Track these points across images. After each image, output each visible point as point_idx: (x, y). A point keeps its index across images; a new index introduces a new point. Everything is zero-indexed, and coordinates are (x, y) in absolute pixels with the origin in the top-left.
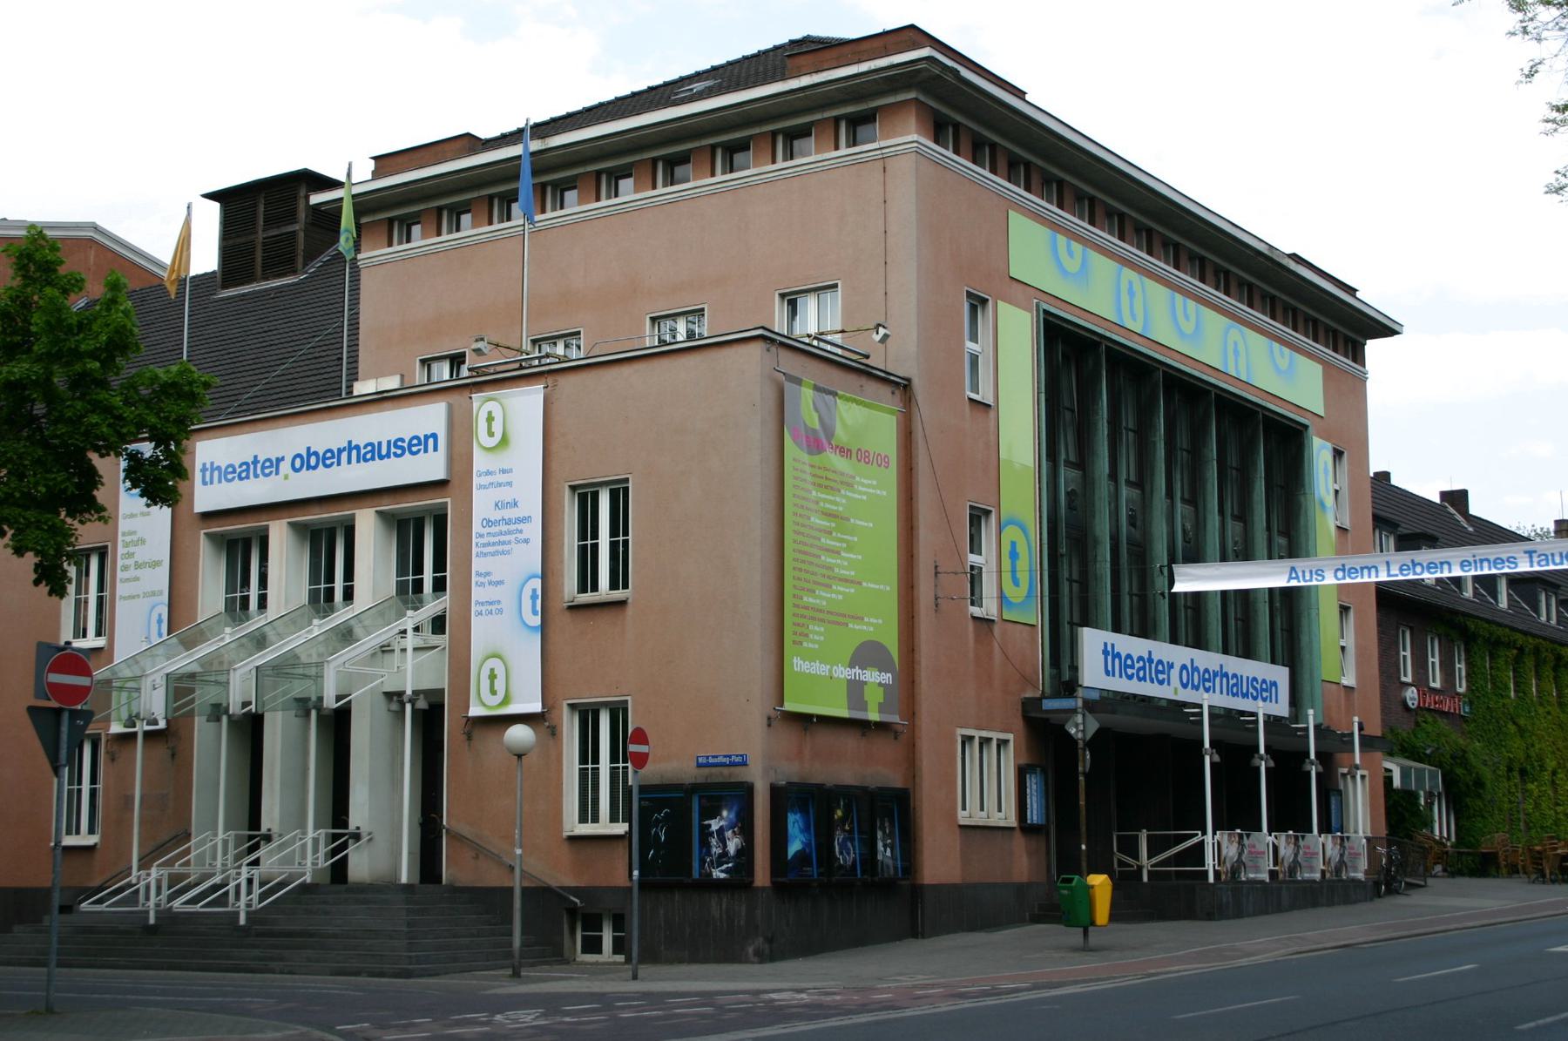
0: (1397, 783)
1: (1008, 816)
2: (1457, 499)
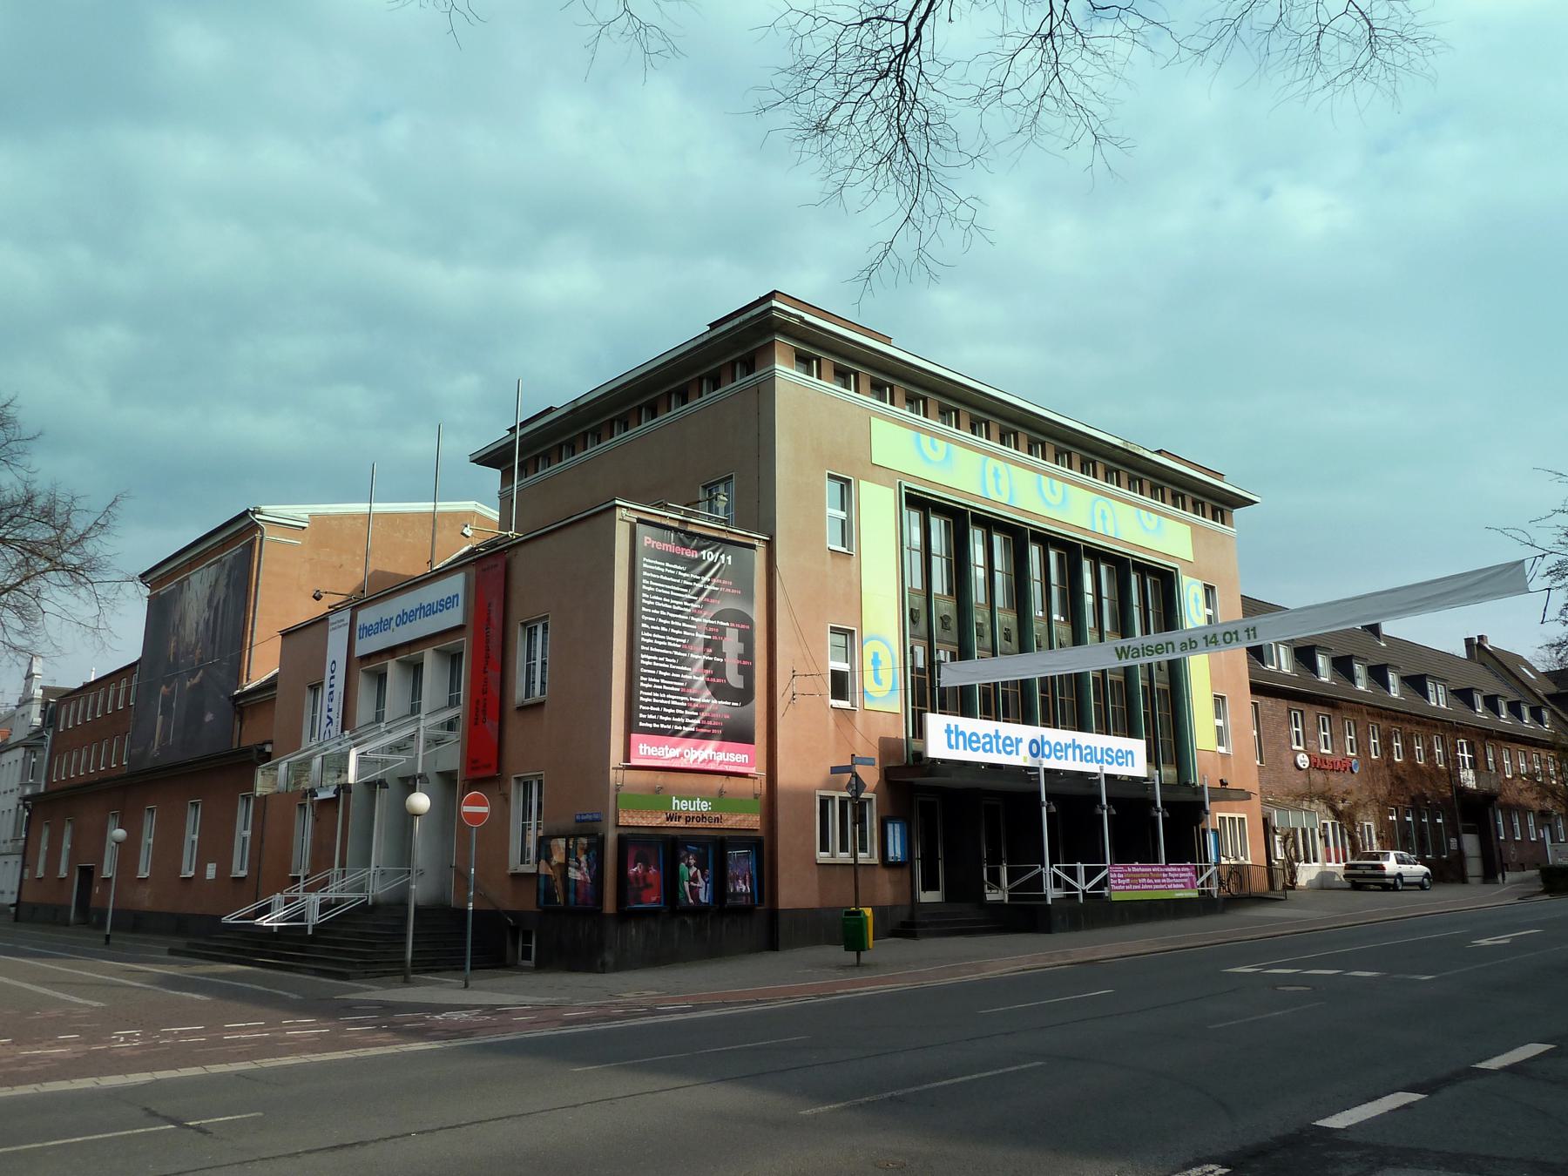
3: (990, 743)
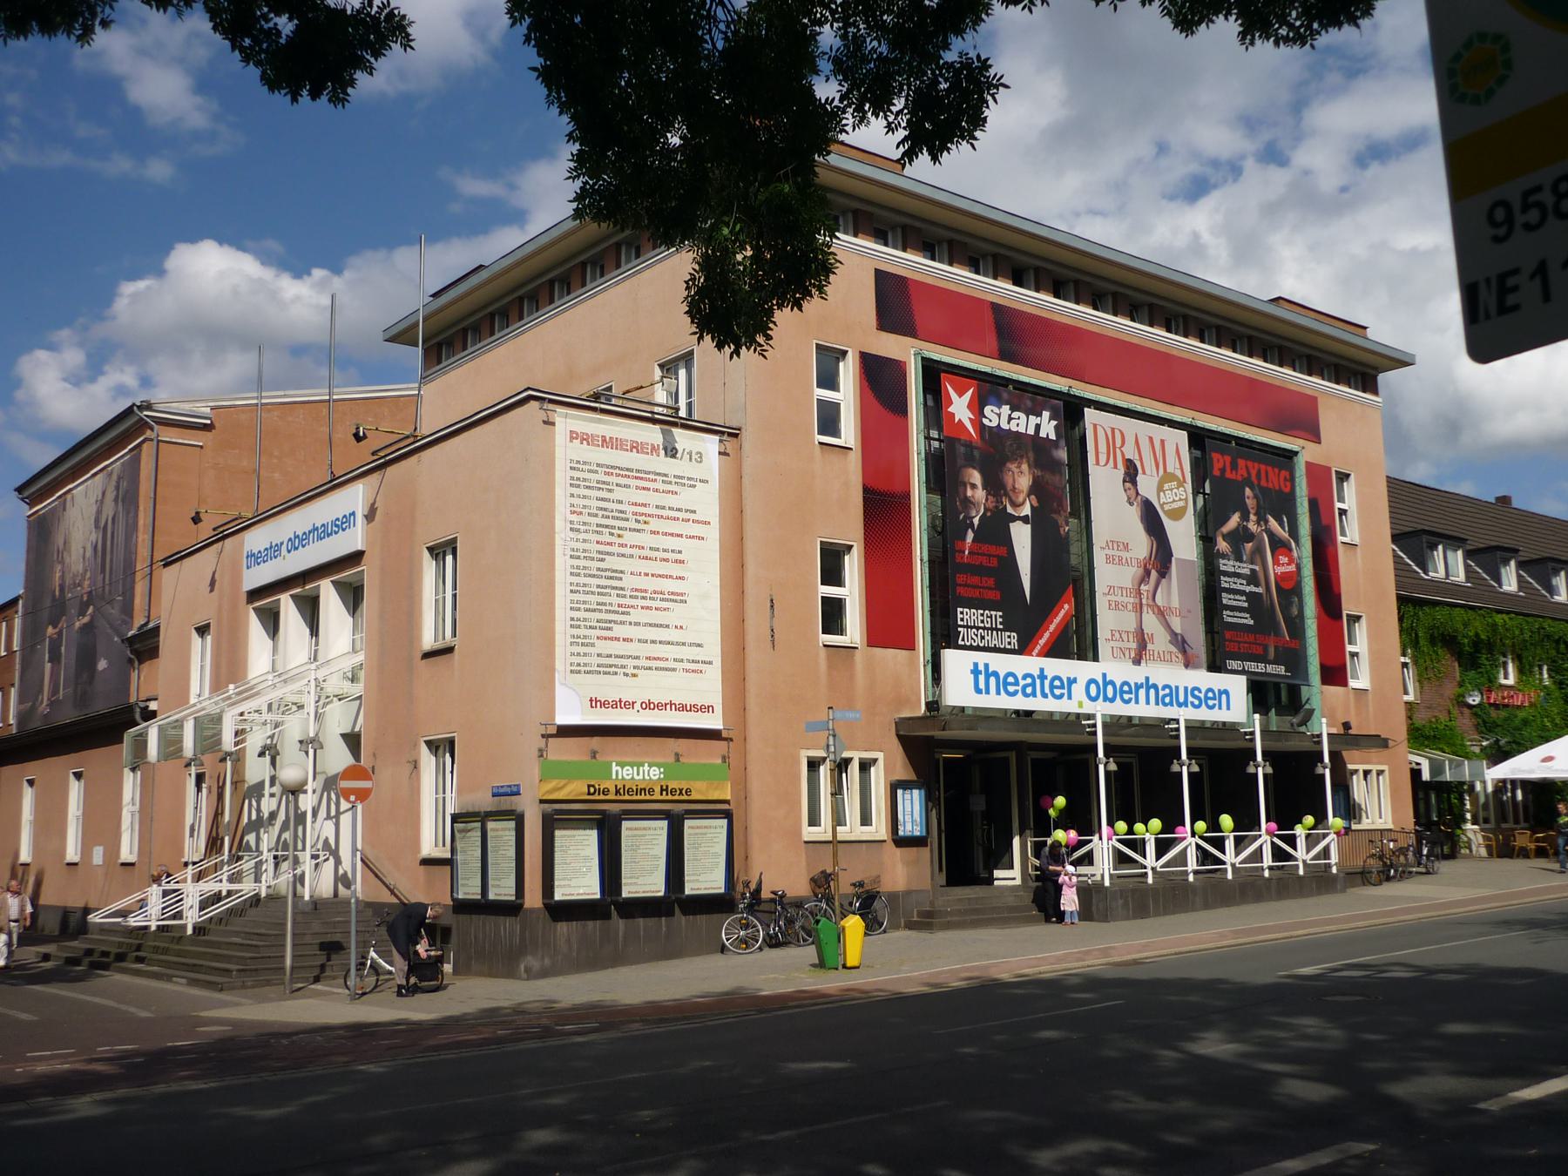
0: (1426, 776)
1: (879, 829)
2: (1504, 500)
3: (1033, 684)
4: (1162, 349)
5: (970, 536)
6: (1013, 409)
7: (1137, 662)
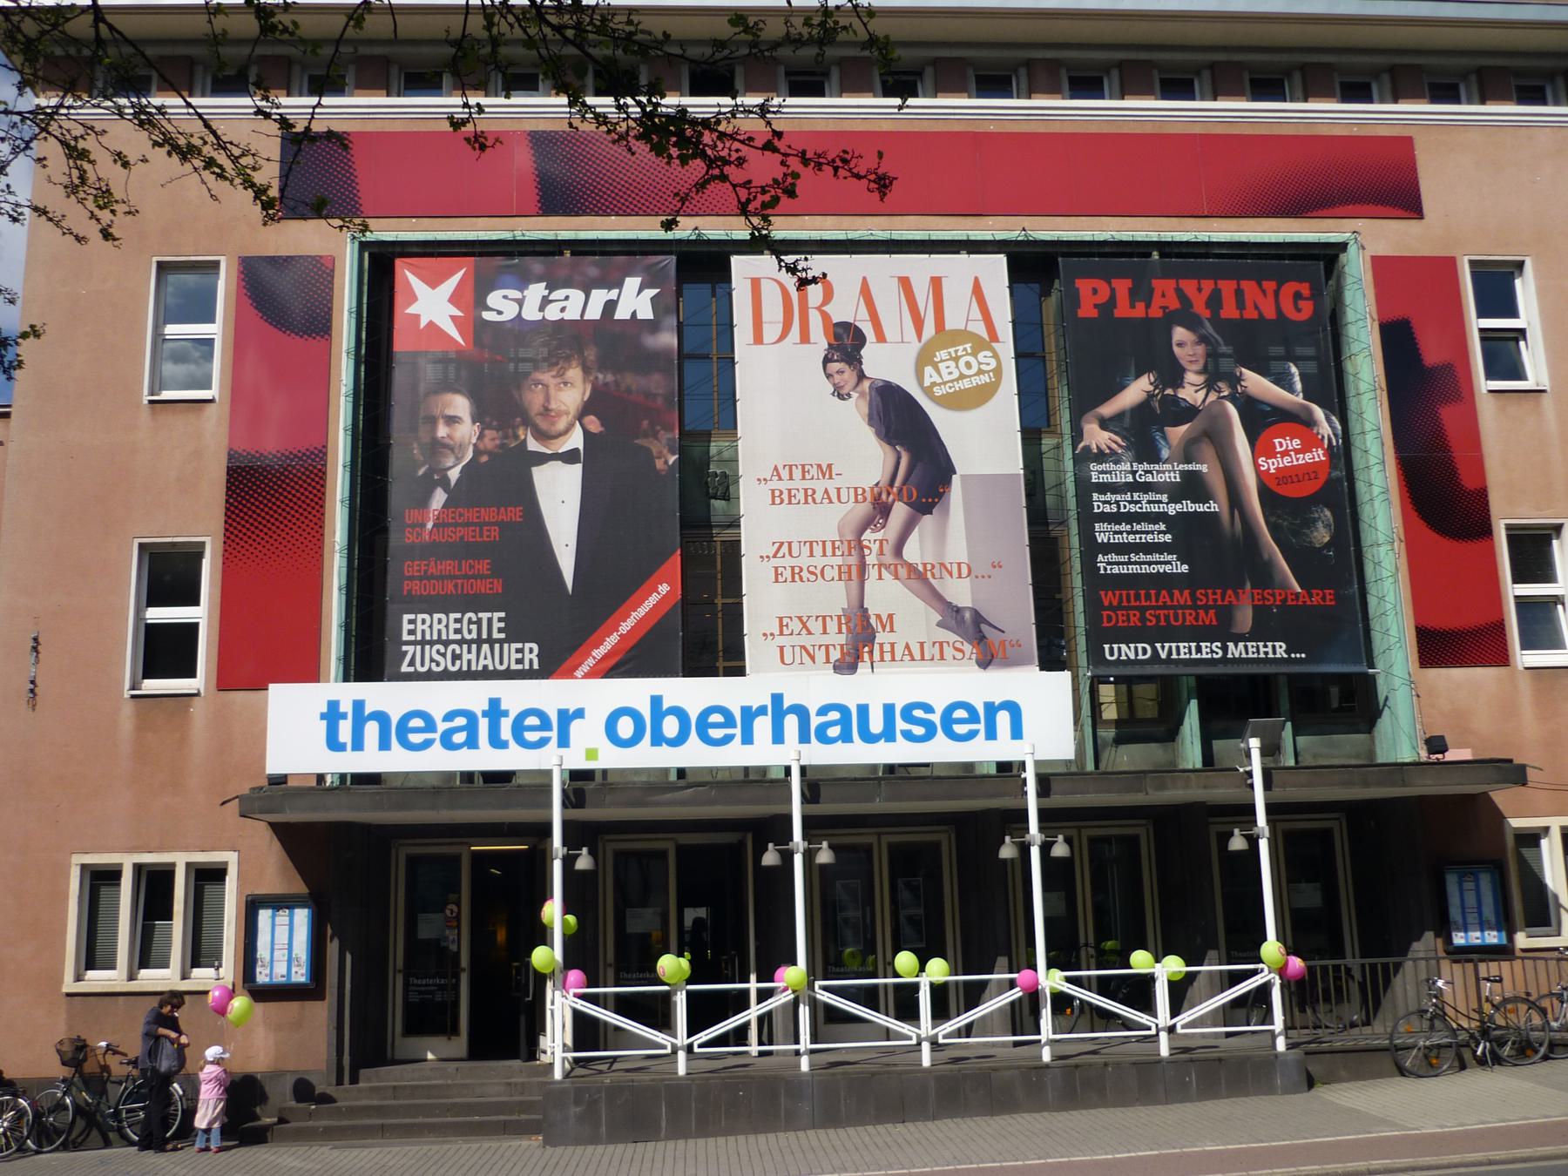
4: (1148, 129)
5: (439, 498)
6: (551, 288)
7: (847, 665)
